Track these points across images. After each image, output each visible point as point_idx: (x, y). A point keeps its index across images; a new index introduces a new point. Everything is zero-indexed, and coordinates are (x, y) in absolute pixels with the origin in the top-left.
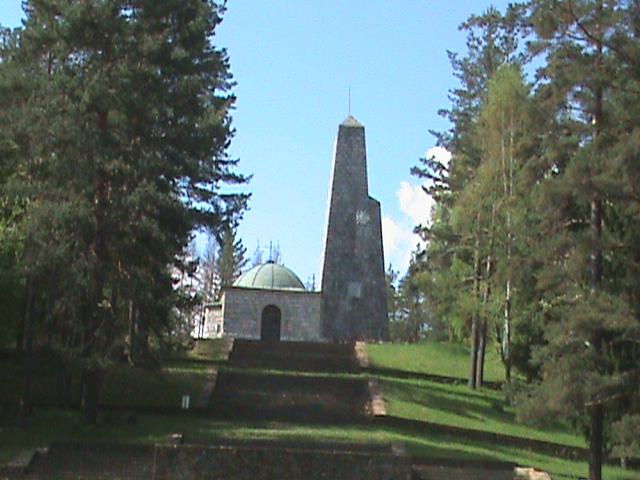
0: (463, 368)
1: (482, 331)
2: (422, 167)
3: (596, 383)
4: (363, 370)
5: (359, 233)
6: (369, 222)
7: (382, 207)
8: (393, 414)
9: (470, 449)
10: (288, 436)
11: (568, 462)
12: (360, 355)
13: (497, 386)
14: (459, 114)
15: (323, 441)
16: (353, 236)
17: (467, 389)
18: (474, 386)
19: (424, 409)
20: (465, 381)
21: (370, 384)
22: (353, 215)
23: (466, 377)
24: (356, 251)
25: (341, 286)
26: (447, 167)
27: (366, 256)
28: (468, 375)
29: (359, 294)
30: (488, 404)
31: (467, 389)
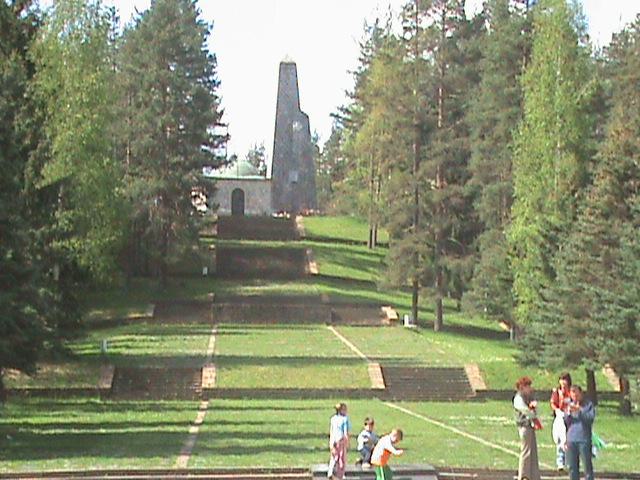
2: (336, 112)
4: (303, 238)
5: (295, 137)
8: (322, 273)
15: (286, 294)
18: (371, 247)
19: (340, 268)
20: (365, 243)
21: (308, 252)
24: (294, 150)
25: (284, 174)
27: (300, 153)
29: (296, 179)
30: (378, 260)
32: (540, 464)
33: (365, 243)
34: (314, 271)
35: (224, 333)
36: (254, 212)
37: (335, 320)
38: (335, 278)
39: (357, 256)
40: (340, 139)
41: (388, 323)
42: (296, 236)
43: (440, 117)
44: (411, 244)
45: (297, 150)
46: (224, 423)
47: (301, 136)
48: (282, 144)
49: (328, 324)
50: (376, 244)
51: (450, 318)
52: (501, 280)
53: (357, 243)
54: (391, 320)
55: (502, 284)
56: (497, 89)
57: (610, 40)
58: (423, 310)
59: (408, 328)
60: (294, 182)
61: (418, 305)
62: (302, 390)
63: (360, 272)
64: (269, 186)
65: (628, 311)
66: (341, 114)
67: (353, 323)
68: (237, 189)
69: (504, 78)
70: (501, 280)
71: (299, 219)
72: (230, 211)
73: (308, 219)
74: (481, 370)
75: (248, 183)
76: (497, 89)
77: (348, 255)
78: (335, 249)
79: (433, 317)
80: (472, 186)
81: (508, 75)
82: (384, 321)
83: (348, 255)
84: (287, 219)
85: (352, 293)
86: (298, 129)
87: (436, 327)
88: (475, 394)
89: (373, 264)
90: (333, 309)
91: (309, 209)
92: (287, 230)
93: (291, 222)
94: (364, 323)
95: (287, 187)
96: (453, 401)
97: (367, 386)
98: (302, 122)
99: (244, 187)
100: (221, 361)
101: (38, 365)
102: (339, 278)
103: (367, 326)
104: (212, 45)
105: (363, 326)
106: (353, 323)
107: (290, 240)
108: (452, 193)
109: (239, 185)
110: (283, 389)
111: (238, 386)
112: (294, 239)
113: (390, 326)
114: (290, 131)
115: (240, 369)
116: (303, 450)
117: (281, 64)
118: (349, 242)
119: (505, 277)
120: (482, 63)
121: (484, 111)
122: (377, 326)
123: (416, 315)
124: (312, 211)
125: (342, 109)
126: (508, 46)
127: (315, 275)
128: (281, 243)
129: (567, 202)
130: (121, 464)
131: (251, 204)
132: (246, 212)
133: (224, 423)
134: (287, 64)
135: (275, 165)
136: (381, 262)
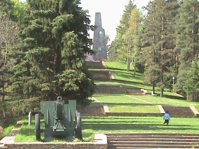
0: (125, 67)
1: (130, 60)
2: (117, 28)
3: (154, 77)
4: (106, 68)
5: (100, 36)
6: (102, 34)
7: (105, 31)
8: (116, 79)
9: (131, 85)
10: (105, 84)
11: (147, 87)
12: (104, 64)
13: (133, 71)
14: (124, 16)
15: (108, 85)
16: (99, 37)
17: (126, 72)
18: (128, 71)
19: (121, 77)
20: (126, 70)
21: (110, 72)
22: (99, 33)
23: (126, 69)
24: (100, 40)
25: (97, 48)
26: (165, 113)
27: (102, 41)
28: (127, 69)
29: (100, 50)
30: (132, 75)
31: (126, 72)
33: (126, 70)
34: (113, 78)
35: (97, 97)
37: (128, 93)
38: (122, 80)
39: (124, 74)
40: (108, 38)
41: (145, 94)
42: (103, 67)
43: (162, 27)
44: (154, 68)
45: (101, 41)
46: (136, 122)
47: (102, 36)
48: (96, 39)
49: (126, 94)
50: (129, 70)
51: (165, 93)
52: (193, 79)
53: (123, 70)
54: (146, 93)
55: (194, 80)
56: (185, 17)
57: (85, 10)
58: (156, 91)
59: (153, 96)
61: (155, 90)
62: (138, 113)
63: (127, 79)
67: (134, 94)
69: (187, 14)
70: (193, 79)
71: (103, 62)
73: (106, 62)
74: (196, 108)
76: (185, 17)
77: (122, 73)
78: (117, 72)
79: (160, 93)
80: (176, 49)
81: (189, 13)
82: (143, 94)
83: (122, 73)
84: (98, 62)
85: (127, 85)
86: (101, 34)
87: (161, 95)
88: (196, 116)
89: (130, 76)
90: (127, 90)
91: (105, 59)
92: (100, 66)
93: (101, 63)
94: (137, 94)
96: (189, 118)
97: (160, 112)
98: (102, 32)
100: (109, 104)
102: (126, 81)
103: (138, 95)
105: (137, 95)
106: (134, 94)
107: (102, 69)
108: (168, 51)
110: (132, 113)
111: (117, 112)
112: (103, 69)
113: (146, 95)
115: (115, 107)
116: (185, 129)
117: (96, 13)
118: (121, 70)
119: (195, 78)
120: (179, 9)
121: (180, 25)
122: (141, 95)
123: (154, 92)
124: (105, 60)
126: (189, 3)
127: (113, 79)
128: (99, 70)
130: (113, 132)
133: (136, 122)
134: (98, 13)
136: (133, 76)
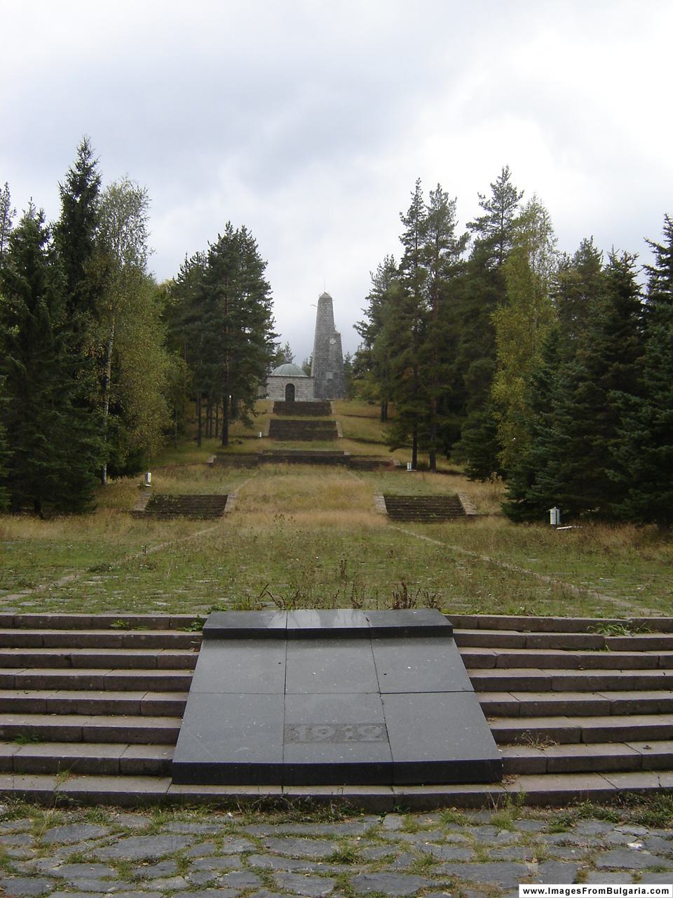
25: (322, 374)
32: (437, 463)
36: (301, 400)
45: (332, 358)
60: (330, 380)
64: (312, 382)
65: (588, 422)
66: (361, 327)
68: (288, 385)
72: (284, 399)
75: (297, 380)
87: (409, 466)
95: (325, 383)
99: (295, 382)
101: (484, 553)
104: (267, 276)
109: (290, 381)
114: (327, 344)
125: (362, 324)
129: (542, 214)
131: (299, 394)
132: (296, 399)
135: (558, 647)
